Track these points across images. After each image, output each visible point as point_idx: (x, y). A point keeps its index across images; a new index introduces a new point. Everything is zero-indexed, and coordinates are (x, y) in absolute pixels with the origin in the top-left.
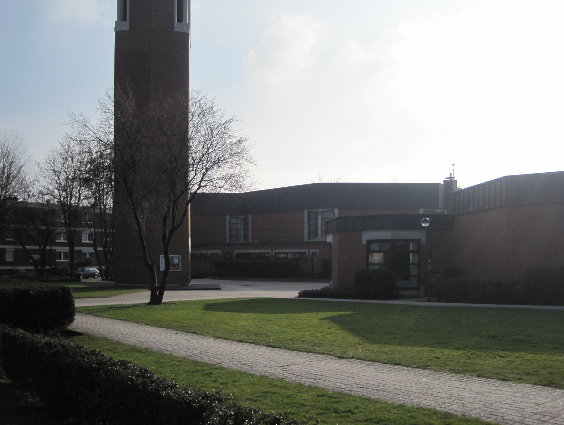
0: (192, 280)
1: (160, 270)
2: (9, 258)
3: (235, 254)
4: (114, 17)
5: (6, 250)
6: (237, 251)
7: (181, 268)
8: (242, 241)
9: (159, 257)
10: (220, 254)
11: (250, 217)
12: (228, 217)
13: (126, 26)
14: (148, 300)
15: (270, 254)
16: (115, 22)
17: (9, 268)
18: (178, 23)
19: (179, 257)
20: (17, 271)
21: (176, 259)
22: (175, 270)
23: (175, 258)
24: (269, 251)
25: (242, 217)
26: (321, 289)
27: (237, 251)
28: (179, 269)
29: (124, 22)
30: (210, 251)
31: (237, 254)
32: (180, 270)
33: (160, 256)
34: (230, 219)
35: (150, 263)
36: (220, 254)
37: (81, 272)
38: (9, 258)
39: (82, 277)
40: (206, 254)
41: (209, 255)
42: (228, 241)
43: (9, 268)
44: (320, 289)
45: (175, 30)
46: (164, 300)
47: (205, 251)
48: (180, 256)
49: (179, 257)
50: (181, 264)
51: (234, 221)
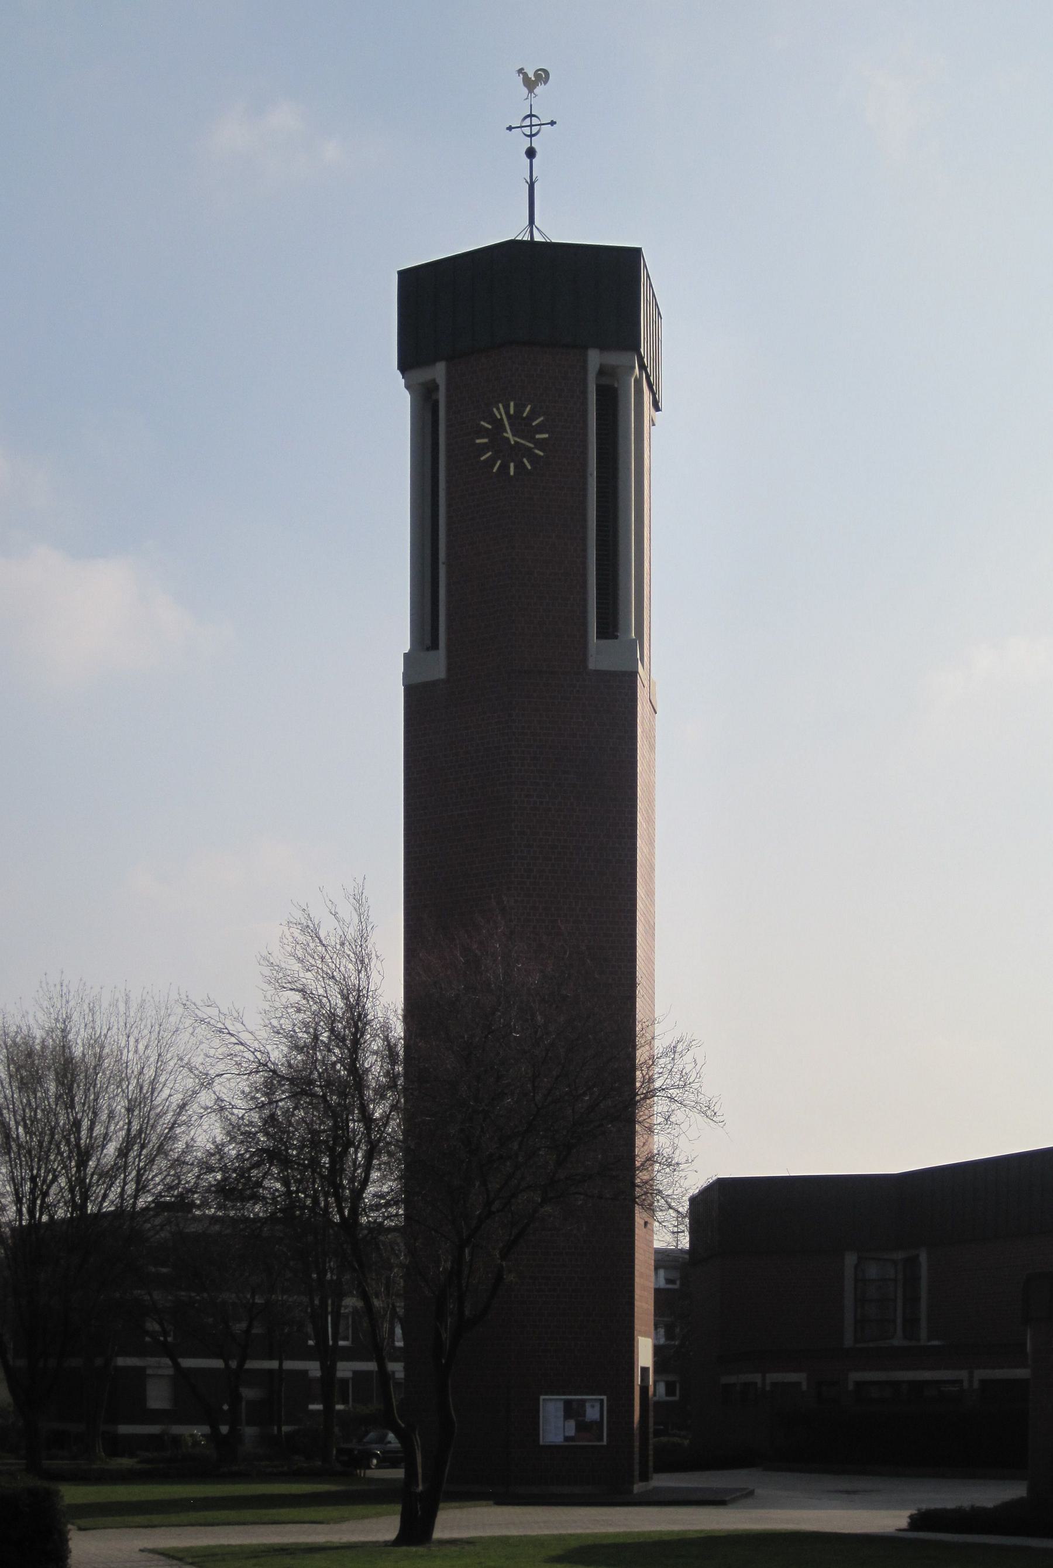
0: (655, 1476)
1: (539, 1443)
2: (158, 1397)
3: (851, 1387)
4: (402, 640)
5: (149, 1372)
6: (855, 1376)
7: (608, 1435)
8: (898, 1341)
9: (538, 1399)
10: (804, 1387)
11: (923, 1258)
12: (850, 1259)
13: (437, 667)
14: (391, 1535)
15: (966, 1385)
16: (405, 654)
17: (155, 1429)
18: (603, 642)
19: (602, 1401)
20: (176, 1440)
21: (593, 1406)
22: (590, 1444)
23: (588, 1405)
24: (963, 1375)
25: (899, 1255)
26: (994, 1506)
27: (855, 1376)
28: (601, 1439)
29: (432, 653)
30: (773, 1377)
31: (858, 1384)
32: (605, 1443)
33: (542, 1397)
34: (856, 1267)
35: (403, 1425)
36: (804, 1387)
37: (374, 1446)
38: (158, 1397)
39: (375, 1461)
40: (759, 1385)
41: (768, 1388)
42: (849, 1341)
43: (155, 1429)
44: (990, 1505)
45: (591, 666)
46: (437, 1534)
47: (757, 1378)
48: (604, 1398)
49: (602, 1401)
50: (608, 1422)
51: (872, 1271)
